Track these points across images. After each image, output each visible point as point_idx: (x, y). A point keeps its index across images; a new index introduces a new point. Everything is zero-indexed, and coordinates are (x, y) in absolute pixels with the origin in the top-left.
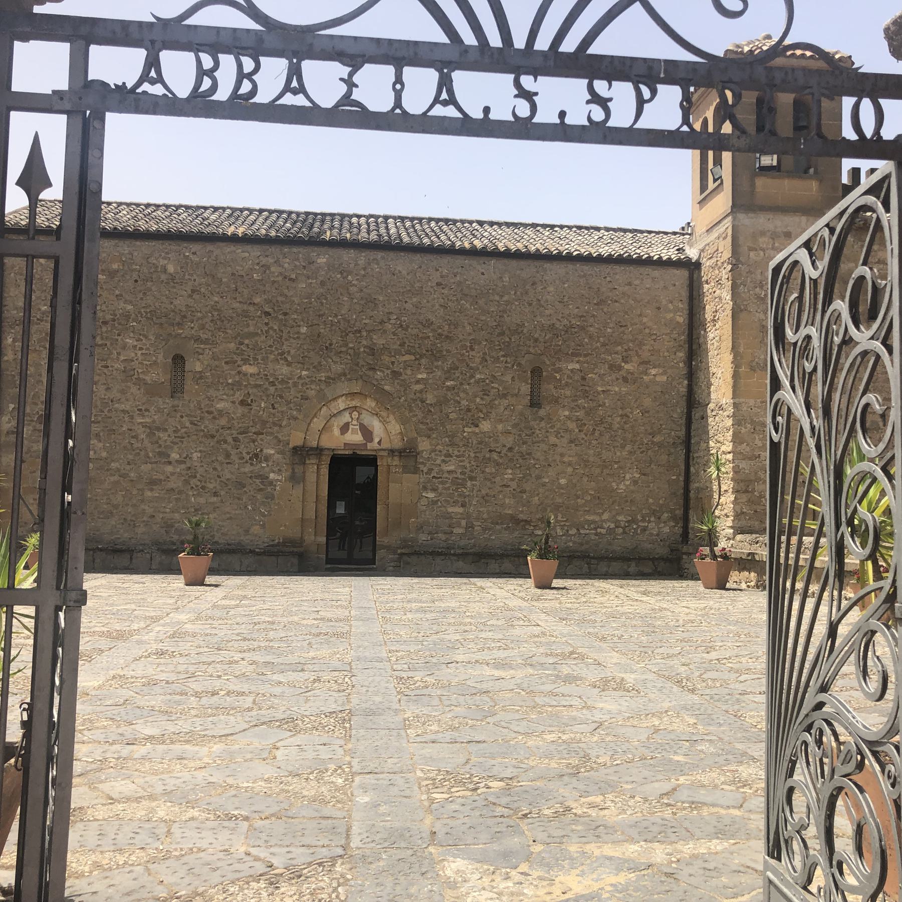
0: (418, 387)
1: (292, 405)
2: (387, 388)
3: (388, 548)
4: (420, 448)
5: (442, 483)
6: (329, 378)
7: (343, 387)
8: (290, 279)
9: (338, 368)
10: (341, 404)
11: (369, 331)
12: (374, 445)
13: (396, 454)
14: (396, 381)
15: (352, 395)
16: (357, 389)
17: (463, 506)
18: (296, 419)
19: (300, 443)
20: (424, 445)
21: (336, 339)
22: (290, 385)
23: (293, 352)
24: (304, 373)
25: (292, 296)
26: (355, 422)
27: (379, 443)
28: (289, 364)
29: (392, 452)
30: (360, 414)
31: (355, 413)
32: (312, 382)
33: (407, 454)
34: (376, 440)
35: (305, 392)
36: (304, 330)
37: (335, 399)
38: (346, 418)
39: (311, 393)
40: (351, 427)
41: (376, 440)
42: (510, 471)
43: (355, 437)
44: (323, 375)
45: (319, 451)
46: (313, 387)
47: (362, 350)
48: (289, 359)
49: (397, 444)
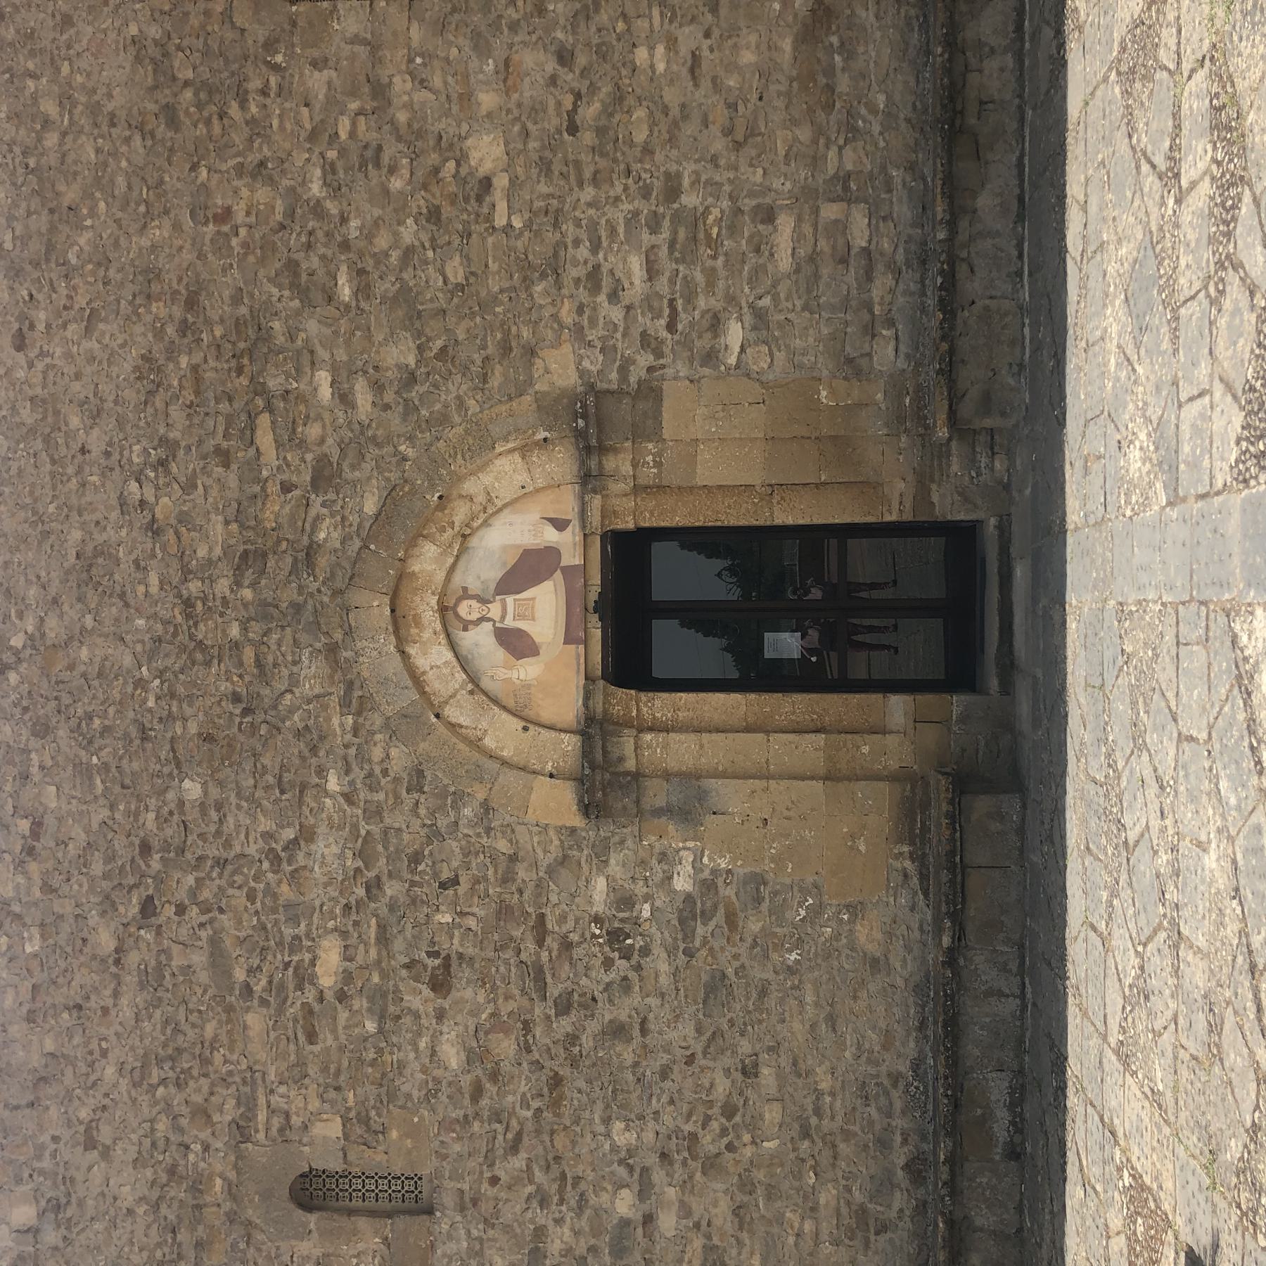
0: (363, 397)
1: (442, 822)
2: (370, 507)
3: (923, 482)
5: (690, 299)
6: (345, 703)
7: (375, 652)
9: (312, 673)
10: (432, 657)
11: (186, 573)
12: (569, 545)
13: (593, 463)
14: (348, 474)
15: (400, 622)
16: (379, 609)
17: (768, 215)
18: (486, 807)
20: (561, 369)
21: (219, 681)
22: (375, 829)
23: (265, 824)
24: (333, 784)
25: (88, 831)
26: (494, 611)
27: (560, 525)
28: (307, 834)
29: (589, 480)
30: (465, 594)
31: (463, 610)
32: (362, 757)
33: (594, 425)
34: (551, 535)
35: (397, 780)
36: (192, 789)
37: (417, 679)
38: (480, 641)
39: (400, 759)
40: (509, 622)
41: (551, 535)
42: (641, 54)
43: (544, 609)
44: (339, 723)
45: (594, 729)
46: (377, 753)
47: (247, 594)
48: (289, 834)
49: (560, 462)
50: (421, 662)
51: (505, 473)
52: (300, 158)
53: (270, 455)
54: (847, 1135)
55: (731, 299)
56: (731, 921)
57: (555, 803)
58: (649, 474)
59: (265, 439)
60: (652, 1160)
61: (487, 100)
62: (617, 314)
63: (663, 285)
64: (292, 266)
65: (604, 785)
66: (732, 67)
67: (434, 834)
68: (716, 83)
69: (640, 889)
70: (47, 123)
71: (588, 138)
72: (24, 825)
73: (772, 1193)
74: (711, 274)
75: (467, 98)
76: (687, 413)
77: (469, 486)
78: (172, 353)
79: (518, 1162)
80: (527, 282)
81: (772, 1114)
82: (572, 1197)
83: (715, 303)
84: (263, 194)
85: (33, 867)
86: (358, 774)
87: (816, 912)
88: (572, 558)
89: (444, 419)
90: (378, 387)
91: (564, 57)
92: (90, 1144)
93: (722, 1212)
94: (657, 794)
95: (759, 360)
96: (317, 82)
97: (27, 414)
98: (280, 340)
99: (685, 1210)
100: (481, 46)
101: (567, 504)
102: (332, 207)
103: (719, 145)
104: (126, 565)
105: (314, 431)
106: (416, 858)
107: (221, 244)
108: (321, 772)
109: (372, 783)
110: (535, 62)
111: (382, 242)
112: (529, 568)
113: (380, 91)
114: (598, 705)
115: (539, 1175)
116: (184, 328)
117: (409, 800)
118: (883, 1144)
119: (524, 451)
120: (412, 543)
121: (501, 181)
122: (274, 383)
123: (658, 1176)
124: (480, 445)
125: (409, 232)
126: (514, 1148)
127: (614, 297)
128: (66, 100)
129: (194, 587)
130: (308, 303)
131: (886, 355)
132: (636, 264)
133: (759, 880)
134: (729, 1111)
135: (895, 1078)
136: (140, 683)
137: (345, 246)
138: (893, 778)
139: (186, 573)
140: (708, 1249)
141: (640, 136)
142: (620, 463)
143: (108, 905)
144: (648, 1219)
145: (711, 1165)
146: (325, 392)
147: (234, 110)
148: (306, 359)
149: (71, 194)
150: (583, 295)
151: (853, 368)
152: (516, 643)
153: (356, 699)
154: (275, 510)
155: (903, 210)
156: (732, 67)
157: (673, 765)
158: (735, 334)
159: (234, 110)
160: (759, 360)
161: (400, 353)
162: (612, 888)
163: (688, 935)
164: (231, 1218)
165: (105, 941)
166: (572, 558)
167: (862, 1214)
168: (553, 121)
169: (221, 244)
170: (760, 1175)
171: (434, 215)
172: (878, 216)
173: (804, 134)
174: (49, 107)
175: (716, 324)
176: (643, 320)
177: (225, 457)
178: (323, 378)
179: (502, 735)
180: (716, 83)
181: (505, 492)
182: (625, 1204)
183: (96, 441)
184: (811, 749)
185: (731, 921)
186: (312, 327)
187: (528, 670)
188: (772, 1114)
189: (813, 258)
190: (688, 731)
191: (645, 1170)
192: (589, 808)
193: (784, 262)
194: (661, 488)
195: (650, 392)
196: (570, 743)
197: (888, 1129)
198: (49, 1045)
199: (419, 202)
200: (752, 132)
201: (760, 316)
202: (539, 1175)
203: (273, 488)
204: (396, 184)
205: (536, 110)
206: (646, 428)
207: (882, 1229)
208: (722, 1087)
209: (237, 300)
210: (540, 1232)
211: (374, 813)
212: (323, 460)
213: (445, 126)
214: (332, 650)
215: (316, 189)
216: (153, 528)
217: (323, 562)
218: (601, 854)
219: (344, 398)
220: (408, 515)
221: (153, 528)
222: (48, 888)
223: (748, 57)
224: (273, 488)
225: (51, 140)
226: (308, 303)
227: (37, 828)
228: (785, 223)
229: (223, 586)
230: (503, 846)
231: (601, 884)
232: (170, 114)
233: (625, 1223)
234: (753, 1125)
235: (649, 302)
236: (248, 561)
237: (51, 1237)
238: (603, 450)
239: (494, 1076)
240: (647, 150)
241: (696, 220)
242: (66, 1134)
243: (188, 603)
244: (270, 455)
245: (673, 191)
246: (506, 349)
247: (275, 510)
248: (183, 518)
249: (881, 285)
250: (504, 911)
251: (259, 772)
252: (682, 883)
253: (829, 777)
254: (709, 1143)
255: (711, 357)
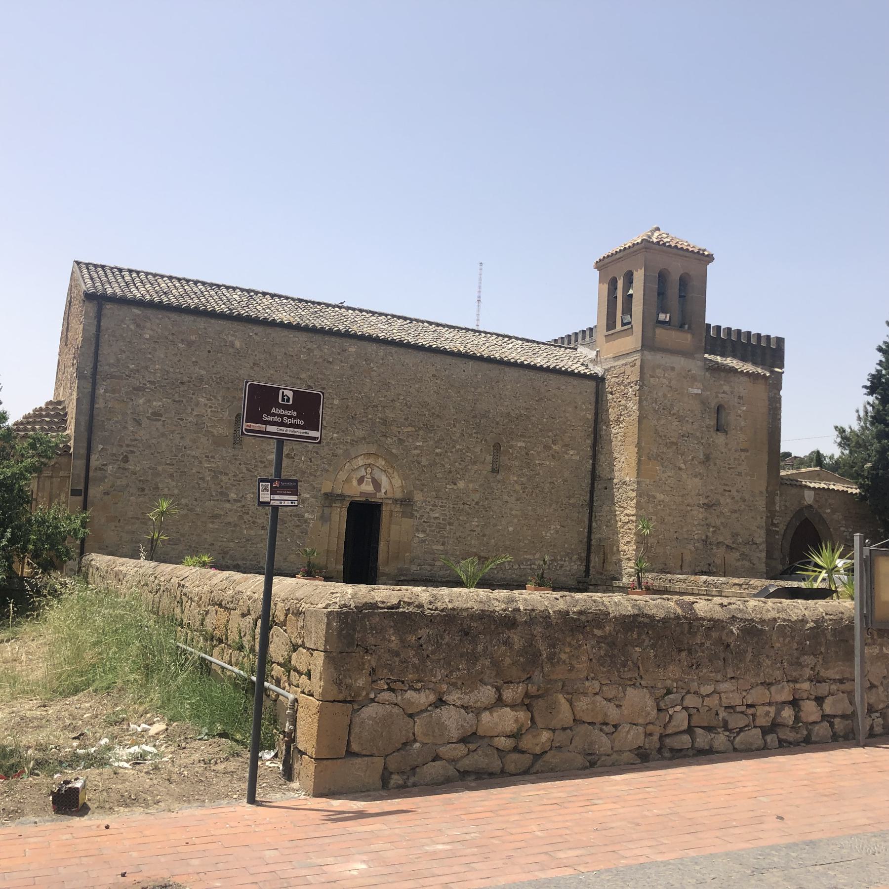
2: (393, 451)
4: (416, 499)
5: (429, 526)
6: (353, 440)
7: (364, 448)
8: (328, 362)
9: (360, 433)
10: (361, 461)
12: (381, 494)
15: (369, 455)
16: (373, 451)
17: (443, 544)
18: (327, 471)
19: (329, 490)
20: (418, 497)
24: (335, 435)
26: (368, 476)
27: (385, 493)
29: (395, 501)
30: (372, 470)
33: (406, 502)
34: (383, 491)
36: (336, 402)
37: (356, 457)
38: (362, 472)
41: (383, 491)
45: (342, 497)
46: (341, 446)
49: (399, 495)
50: (359, 459)
51: (397, 482)
52: (464, 444)
53: (406, 430)
54: (246, 551)
55: (428, 535)
56: (298, 526)
57: (327, 487)
58: (395, 514)
59: (410, 429)
60: (243, 503)
61: (471, 486)
62: (427, 510)
63: (432, 520)
64: (443, 440)
65: (330, 498)
66: (471, 539)
67: (322, 458)
68: (469, 535)
69: (306, 505)
70: (476, 389)
71: (462, 507)
72: (331, 360)
73: (233, 531)
74: (433, 531)
75: (471, 481)
76: (407, 523)
77: (396, 473)
78: (429, 410)
79: (244, 471)
80: (435, 491)
81: (252, 533)
82: (235, 483)
83: (428, 531)
84: (458, 435)
85: (321, 360)
86: (337, 441)
87: (299, 546)
88: (378, 495)
89: (410, 469)
90: (418, 455)
91: (477, 503)
92: (254, 364)
93: (229, 519)
94: (327, 511)
95: (416, 540)
96: (478, 450)
97: (419, 375)
98: (429, 435)
99: (230, 510)
100: (481, 486)
101: (389, 495)
102: (454, 450)
103: (458, 534)
104: (386, 393)
105: (410, 440)
106: (317, 453)
107: (449, 425)
108: (338, 433)
109: (334, 444)
110: (476, 497)
111: (446, 460)
112: (377, 484)
113: (475, 463)
114: (347, 499)
115: (241, 475)
116: (433, 414)
117: (330, 453)
118: (243, 559)
119: (402, 487)
120: (385, 459)
121: (455, 487)
122: (421, 433)
123: (239, 504)
124: (405, 478)
125: (448, 466)
126: (248, 470)
127: (431, 509)
128: (480, 394)
129: (380, 409)
130: (436, 442)
131: (414, 568)
132: (437, 515)
133: (306, 534)
134: (254, 522)
135: (259, 562)
136: (360, 393)
137: (446, 452)
138: (768, 689)
139: (384, 407)
140: (220, 515)
141: (461, 518)
142: (398, 508)
143: (311, 377)
144: (229, 501)
145: (241, 517)
146: (418, 444)
147: (474, 431)
148: (424, 440)
149: (462, 392)
150: (432, 503)
151: (412, 561)
152: (361, 480)
153: (354, 443)
154: (395, 429)
155: (441, 573)
156: (471, 539)
157: (333, 515)
158: (421, 535)
159: (474, 431)
160: (416, 540)
161: (424, 462)
162: (307, 499)
163: (295, 516)
164: (234, 397)
165: (303, 376)
166: (378, 495)
167: (226, 553)
168: (466, 499)
169: (449, 425)
170: (238, 528)
171: (450, 472)
172: (441, 567)
173: (458, 553)
174: (479, 390)
175: (424, 532)
176: (426, 515)
177: (406, 419)
178: (421, 444)
179: (342, 476)
180: (469, 535)
181: (393, 481)
182: (233, 496)
183: (412, 390)
184: (334, 547)
185: (298, 526)
186: (431, 443)
187: (355, 483)
188: (252, 533)
189: (434, 554)
190: (339, 517)
191: (240, 501)
192: (326, 494)
193: (434, 547)
194: (391, 516)
195: (412, 516)
196: (339, 492)
197: (247, 560)
198: (278, 357)
199: (453, 469)
200: (459, 542)
201: (424, 541)
202: (241, 475)
203: (399, 429)
204: (457, 464)
205: (468, 496)
206: (404, 514)
207: (223, 558)
208: (260, 521)
209: (438, 426)
210: (227, 474)
211: (328, 444)
212: (404, 441)
213: (467, 477)
214: (364, 438)
215: (458, 447)
216: (393, 401)
217: (383, 439)
218: (315, 497)
219: (416, 448)
220: (392, 460)
221: (393, 401)
222: (316, 363)
223: (473, 542)
224: (399, 429)
225: (473, 390)
226: (436, 442)
227: (331, 363)
228: (441, 548)
229: (380, 415)
230: (318, 474)
231: (308, 496)
232: (475, 417)
233: (228, 495)
234: (250, 528)
235: (429, 517)
236: (384, 421)
237: (231, 350)
238: (401, 504)
239: (265, 467)
240: (458, 519)
241: (444, 529)
242: (257, 358)
243: (377, 407)
244: (406, 430)
245: (450, 524)
246: (423, 485)
247: (395, 429)
248: (395, 408)
249: (428, 568)
250: (303, 472)
251: (339, 418)
252: (307, 515)
253: (328, 551)
254: (246, 517)
255: (417, 530)
